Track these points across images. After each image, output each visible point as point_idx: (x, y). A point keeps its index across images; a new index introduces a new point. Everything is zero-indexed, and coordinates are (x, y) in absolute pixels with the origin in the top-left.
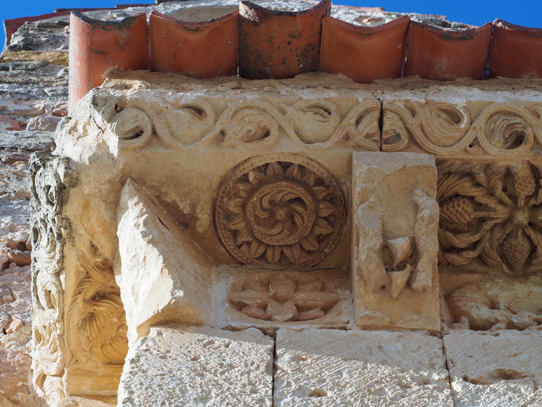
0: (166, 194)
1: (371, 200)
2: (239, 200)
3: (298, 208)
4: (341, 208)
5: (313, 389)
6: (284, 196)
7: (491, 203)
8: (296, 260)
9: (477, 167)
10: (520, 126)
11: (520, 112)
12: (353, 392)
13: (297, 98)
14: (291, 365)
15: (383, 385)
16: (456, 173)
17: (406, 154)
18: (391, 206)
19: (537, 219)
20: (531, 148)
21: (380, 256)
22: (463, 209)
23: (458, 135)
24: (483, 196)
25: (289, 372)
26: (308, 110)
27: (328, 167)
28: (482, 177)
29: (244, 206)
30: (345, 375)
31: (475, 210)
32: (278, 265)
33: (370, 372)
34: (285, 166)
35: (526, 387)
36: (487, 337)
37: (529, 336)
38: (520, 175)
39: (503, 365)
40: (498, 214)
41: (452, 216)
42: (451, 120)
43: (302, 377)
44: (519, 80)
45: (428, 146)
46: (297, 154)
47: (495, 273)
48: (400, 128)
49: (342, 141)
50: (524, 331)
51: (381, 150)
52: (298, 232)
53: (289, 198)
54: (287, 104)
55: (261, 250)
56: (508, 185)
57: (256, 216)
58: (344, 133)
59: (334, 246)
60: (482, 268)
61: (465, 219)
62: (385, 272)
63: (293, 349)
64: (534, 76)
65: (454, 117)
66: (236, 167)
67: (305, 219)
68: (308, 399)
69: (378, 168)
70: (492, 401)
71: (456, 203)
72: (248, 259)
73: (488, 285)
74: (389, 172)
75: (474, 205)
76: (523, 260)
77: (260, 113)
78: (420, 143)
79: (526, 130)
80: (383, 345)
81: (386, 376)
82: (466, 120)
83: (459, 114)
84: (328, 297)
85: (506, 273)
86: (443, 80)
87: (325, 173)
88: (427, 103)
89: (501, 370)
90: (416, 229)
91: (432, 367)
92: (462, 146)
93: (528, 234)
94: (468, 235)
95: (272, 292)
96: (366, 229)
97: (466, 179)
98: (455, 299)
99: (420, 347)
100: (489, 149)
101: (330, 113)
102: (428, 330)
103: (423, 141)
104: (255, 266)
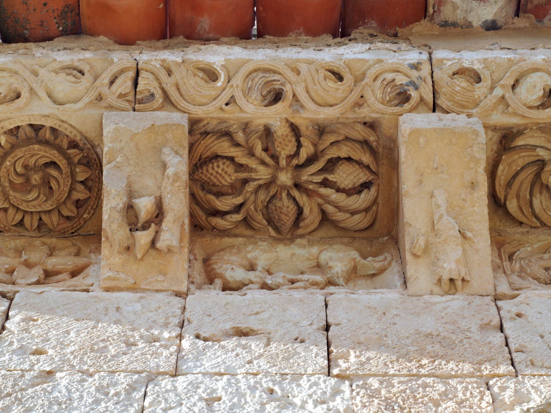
1: (118, 160)
3: (53, 172)
4: (97, 172)
5: (34, 348)
6: (38, 159)
7: (252, 163)
8: (55, 226)
9: (235, 126)
10: (279, 83)
11: (279, 68)
12: (75, 350)
13: (51, 60)
14: (20, 325)
15: (108, 343)
16: (213, 133)
17: (158, 113)
18: (141, 164)
20: (290, 106)
21: (123, 216)
22: (223, 170)
23: (214, 93)
24: (243, 156)
25: (16, 332)
26: (61, 71)
27: (80, 129)
28: (240, 137)
30: (72, 334)
31: (236, 171)
32: (37, 231)
33: (99, 331)
34: (36, 128)
35: (258, 343)
36: (234, 297)
37: (277, 296)
38: (279, 133)
39: (241, 323)
40: (260, 175)
41: (212, 178)
42: (207, 79)
43: (27, 336)
44: (286, 38)
45: (182, 104)
46: (48, 116)
47: (261, 237)
48: (155, 88)
49: (94, 101)
51: (134, 110)
52: (55, 197)
53: (43, 162)
54: (40, 66)
55: (19, 217)
56: (269, 144)
57: (11, 182)
58: (96, 94)
59: (93, 211)
60: (248, 232)
61: (226, 181)
62: (129, 232)
63: (27, 310)
64: (301, 34)
65: (211, 75)
67: (61, 184)
68: (26, 358)
69: (125, 127)
70: (218, 356)
71: (215, 164)
72: (5, 226)
73: (250, 248)
74: (137, 131)
75: (236, 166)
76: (289, 223)
77: (12, 76)
78: (174, 103)
79: (284, 86)
80: (121, 306)
81: (115, 335)
82: (222, 78)
83: (217, 72)
84: (80, 261)
86: (206, 40)
87: (78, 135)
88: (183, 62)
89: (238, 328)
90: (162, 188)
91: (166, 325)
92: (218, 104)
93: (293, 195)
94: (230, 197)
95: (24, 257)
96: (109, 188)
97: (224, 139)
98: (212, 262)
99: (159, 307)
100: (246, 107)
101: (83, 74)
102: (173, 291)
103: (177, 100)
104: (13, 234)
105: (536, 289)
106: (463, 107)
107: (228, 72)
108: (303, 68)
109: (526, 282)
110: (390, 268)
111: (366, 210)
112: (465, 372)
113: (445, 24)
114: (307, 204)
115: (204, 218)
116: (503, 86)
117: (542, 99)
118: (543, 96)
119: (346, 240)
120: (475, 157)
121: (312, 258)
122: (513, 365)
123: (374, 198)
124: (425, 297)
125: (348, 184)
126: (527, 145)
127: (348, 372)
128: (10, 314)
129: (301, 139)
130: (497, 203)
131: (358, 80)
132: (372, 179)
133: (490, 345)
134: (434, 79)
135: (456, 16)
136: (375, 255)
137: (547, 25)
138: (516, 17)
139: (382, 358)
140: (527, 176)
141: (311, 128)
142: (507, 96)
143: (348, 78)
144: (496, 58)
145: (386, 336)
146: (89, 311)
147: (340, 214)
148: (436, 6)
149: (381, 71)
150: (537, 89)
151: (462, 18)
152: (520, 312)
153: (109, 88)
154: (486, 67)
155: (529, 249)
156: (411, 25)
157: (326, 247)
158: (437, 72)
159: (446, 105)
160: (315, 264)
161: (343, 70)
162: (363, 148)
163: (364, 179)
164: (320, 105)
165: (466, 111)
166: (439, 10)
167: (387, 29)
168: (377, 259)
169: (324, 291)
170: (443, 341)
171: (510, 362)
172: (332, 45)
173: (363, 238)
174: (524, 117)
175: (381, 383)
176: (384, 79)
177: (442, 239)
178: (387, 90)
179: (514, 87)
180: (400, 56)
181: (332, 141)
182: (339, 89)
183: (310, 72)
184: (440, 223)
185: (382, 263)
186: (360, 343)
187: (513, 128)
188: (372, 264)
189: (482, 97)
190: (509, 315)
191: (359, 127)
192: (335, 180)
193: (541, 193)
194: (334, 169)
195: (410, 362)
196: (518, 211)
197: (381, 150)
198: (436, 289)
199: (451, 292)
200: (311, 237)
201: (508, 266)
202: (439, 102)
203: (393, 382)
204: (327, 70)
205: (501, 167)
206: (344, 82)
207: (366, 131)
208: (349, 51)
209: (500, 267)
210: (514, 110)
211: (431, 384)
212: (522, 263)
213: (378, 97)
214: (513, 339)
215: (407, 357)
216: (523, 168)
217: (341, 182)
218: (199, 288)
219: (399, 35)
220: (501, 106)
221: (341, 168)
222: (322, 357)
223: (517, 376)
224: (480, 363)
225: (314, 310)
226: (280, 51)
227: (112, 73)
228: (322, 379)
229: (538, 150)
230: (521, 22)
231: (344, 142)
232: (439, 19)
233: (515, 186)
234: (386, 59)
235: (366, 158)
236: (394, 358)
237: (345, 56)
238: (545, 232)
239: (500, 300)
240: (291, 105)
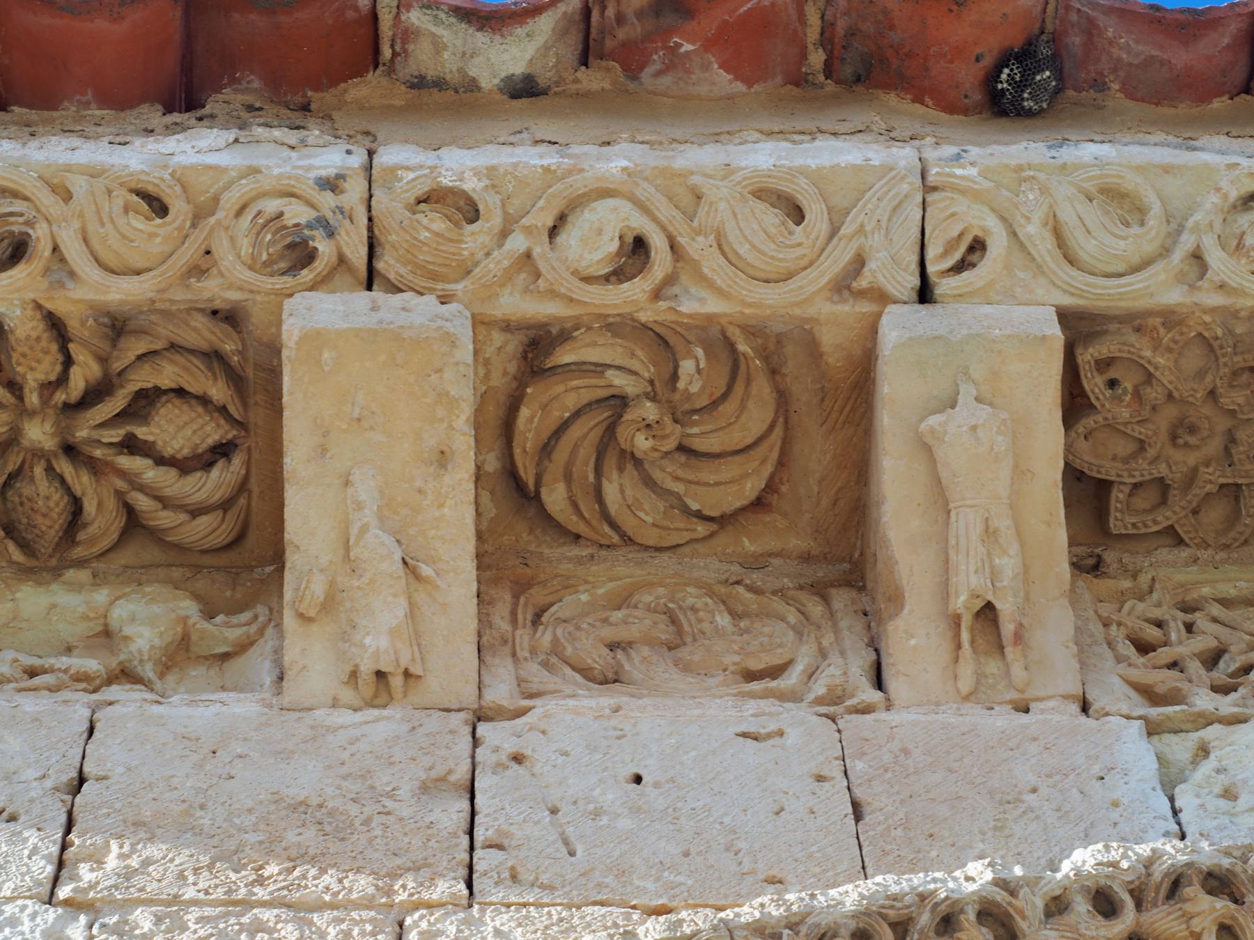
10: (21, 220)
19: (74, 436)
38: (21, 333)
44: (55, 114)
76: (53, 532)
85: (18, 563)
93: (58, 470)
105: (573, 696)
106: (435, 277)
108: (79, 185)
109: (556, 679)
110: (262, 641)
111: (225, 506)
112: (354, 896)
113: (419, 83)
114: (90, 491)
116: (528, 230)
117: (617, 260)
118: (619, 253)
119: (177, 573)
120: (447, 394)
121: (92, 615)
123: (239, 481)
124: (319, 713)
125: (181, 448)
126: (584, 363)
127: (91, 894)
129: (71, 346)
131: (198, 217)
132: (235, 437)
133: (430, 831)
134: (374, 213)
135: (443, 67)
137: (650, 88)
138: (583, 68)
139: (177, 862)
140: (586, 432)
141: (91, 322)
142: (537, 251)
143: (179, 209)
144: (515, 165)
145: (202, 807)
147: (165, 513)
148: (399, 41)
149: (254, 193)
150: (606, 238)
151: (454, 69)
152: (521, 751)
154: (494, 186)
156: (343, 85)
157: (128, 590)
159: (397, 273)
160: (99, 628)
161: (168, 191)
162: (211, 369)
163: (217, 437)
164: (113, 272)
165: (440, 286)
166: (405, 51)
167: (285, 94)
168: (235, 620)
169: (95, 697)
170: (326, 820)
172: (157, 130)
173: (218, 569)
174: (572, 300)
175: (158, 920)
176: (259, 213)
177: (365, 580)
178: (265, 236)
179: (553, 232)
180: (300, 159)
181: (139, 352)
182: (156, 235)
183: (93, 193)
184: (362, 544)
185: (244, 629)
186: (137, 824)
187: (547, 325)
188: (224, 631)
189: (480, 255)
190: (494, 758)
191: (200, 321)
192: (151, 438)
193: (621, 469)
194: (149, 413)
195: (237, 872)
196: (570, 510)
197: (250, 372)
198: (347, 695)
199: (376, 702)
200: (102, 566)
201: (526, 638)
202: (380, 265)
203: (186, 918)
204: (132, 191)
205: (524, 412)
206: (168, 218)
207: (217, 330)
208: (186, 146)
210: (551, 284)
211: (271, 924)
212: (559, 632)
213: (243, 254)
214: (486, 816)
215: (235, 858)
216: (577, 414)
217: (165, 442)
219: (313, 107)
220: (523, 275)
221: (163, 411)
222: (43, 857)
223: (470, 906)
224: (394, 876)
225: (58, 742)
226: (34, 144)
228: (29, 911)
229: (610, 373)
230: (594, 79)
231: (167, 354)
232: (408, 69)
233: (561, 454)
234: (268, 167)
235: (219, 391)
236: (205, 860)
237: (178, 159)
238: (630, 556)
239: (489, 719)
240: (47, 271)
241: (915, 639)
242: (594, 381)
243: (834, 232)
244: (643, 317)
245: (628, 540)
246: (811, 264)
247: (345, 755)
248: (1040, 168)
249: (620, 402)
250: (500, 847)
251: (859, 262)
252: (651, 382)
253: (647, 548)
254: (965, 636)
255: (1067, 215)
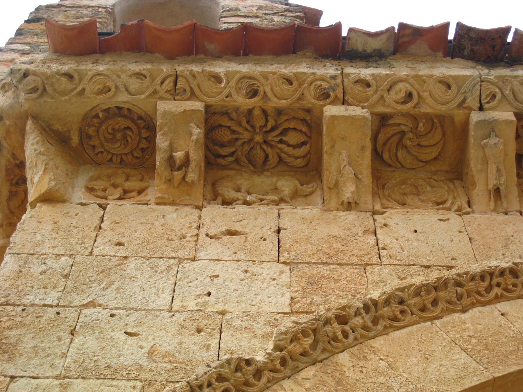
0: (52, 125)
1: (165, 130)
2: (95, 128)
9: (231, 110)
16: (219, 113)
22: (224, 133)
29: (98, 131)
31: (231, 134)
34: (119, 109)
50: (251, 206)
55: (109, 157)
57: (105, 137)
60: (238, 167)
62: (170, 171)
65: (217, 79)
66: (92, 109)
71: (220, 130)
84: (143, 185)
94: (228, 148)
95: (112, 181)
105: (396, 209)
106: (360, 102)
107: (228, 78)
110: (316, 192)
111: (304, 157)
115: (213, 159)
118: (405, 96)
119: (292, 173)
122: (380, 258)
128: (104, 219)
129: (268, 117)
130: (377, 155)
131: (300, 85)
136: (308, 183)
142: (385, 95)
143: (454, 87)
144: (380, 73)
145: (311, 237)
146: (148, 218)
147: (288, 158)
153: (161, 86)
155: (394, 182)
158: (345, 80)
169: (278, 207)
171: (378, 256)
179: (389, 90)
188: (307, 189)
190: (380, 225)
191: (301, 112)
193: (402, 149)
197: (313, 125)
198: (341, 207)
202: (346, 98)
205: (380, 135)
209: (377, 194)
216: (392, 136)
218: (209, 203)
227: (162, 78)
229: (401, 126)
233: (388, 146)
235: (304, 129)
240: (263, 99)
241: (479, 194)
242: (397, 128)
243: (458, 91)
244: (411, 113)
245: (403, 166)
246: (453, 100)
247: (344, 224)
248: (509, 76)
249: (403, 133)
250: (385, 249)
251: (464, 100)
252: (411, 128)
253: (407, 169)
254: (492, 195)
255: (516, 89)
